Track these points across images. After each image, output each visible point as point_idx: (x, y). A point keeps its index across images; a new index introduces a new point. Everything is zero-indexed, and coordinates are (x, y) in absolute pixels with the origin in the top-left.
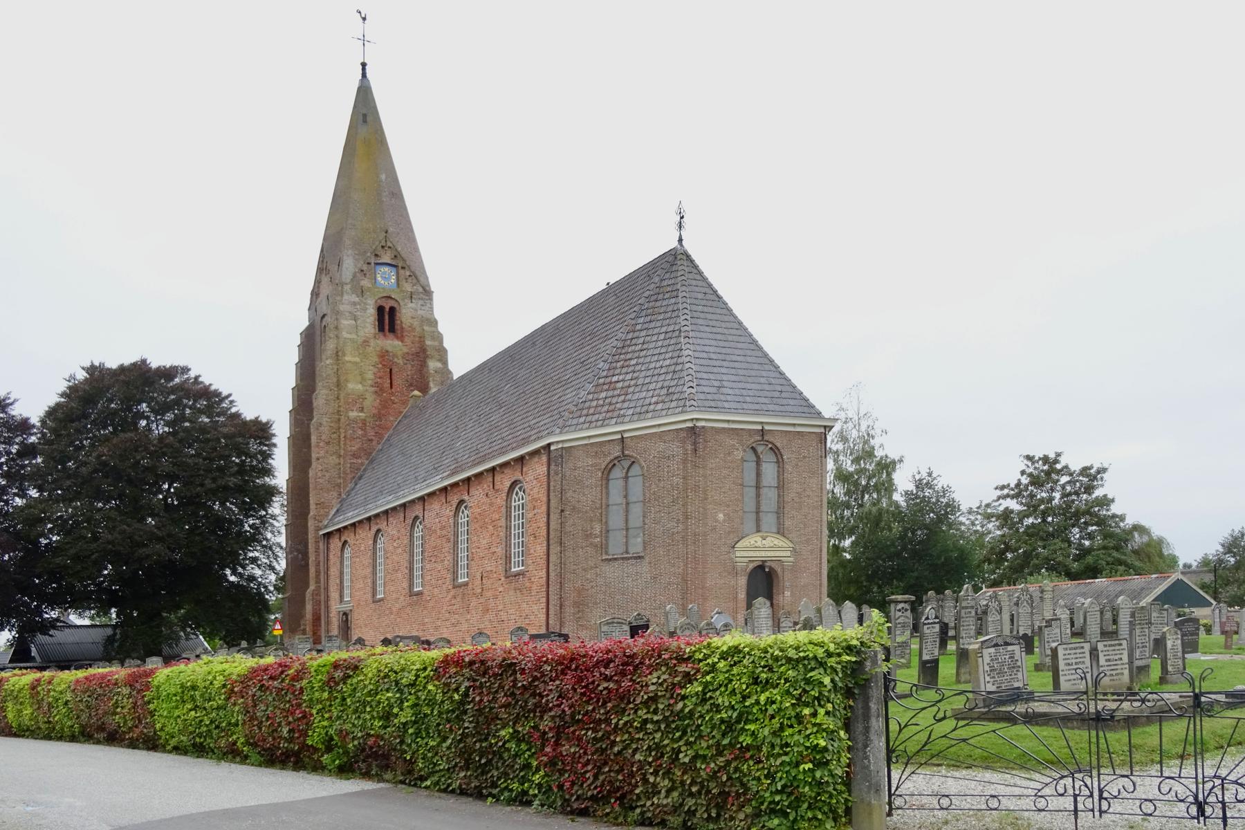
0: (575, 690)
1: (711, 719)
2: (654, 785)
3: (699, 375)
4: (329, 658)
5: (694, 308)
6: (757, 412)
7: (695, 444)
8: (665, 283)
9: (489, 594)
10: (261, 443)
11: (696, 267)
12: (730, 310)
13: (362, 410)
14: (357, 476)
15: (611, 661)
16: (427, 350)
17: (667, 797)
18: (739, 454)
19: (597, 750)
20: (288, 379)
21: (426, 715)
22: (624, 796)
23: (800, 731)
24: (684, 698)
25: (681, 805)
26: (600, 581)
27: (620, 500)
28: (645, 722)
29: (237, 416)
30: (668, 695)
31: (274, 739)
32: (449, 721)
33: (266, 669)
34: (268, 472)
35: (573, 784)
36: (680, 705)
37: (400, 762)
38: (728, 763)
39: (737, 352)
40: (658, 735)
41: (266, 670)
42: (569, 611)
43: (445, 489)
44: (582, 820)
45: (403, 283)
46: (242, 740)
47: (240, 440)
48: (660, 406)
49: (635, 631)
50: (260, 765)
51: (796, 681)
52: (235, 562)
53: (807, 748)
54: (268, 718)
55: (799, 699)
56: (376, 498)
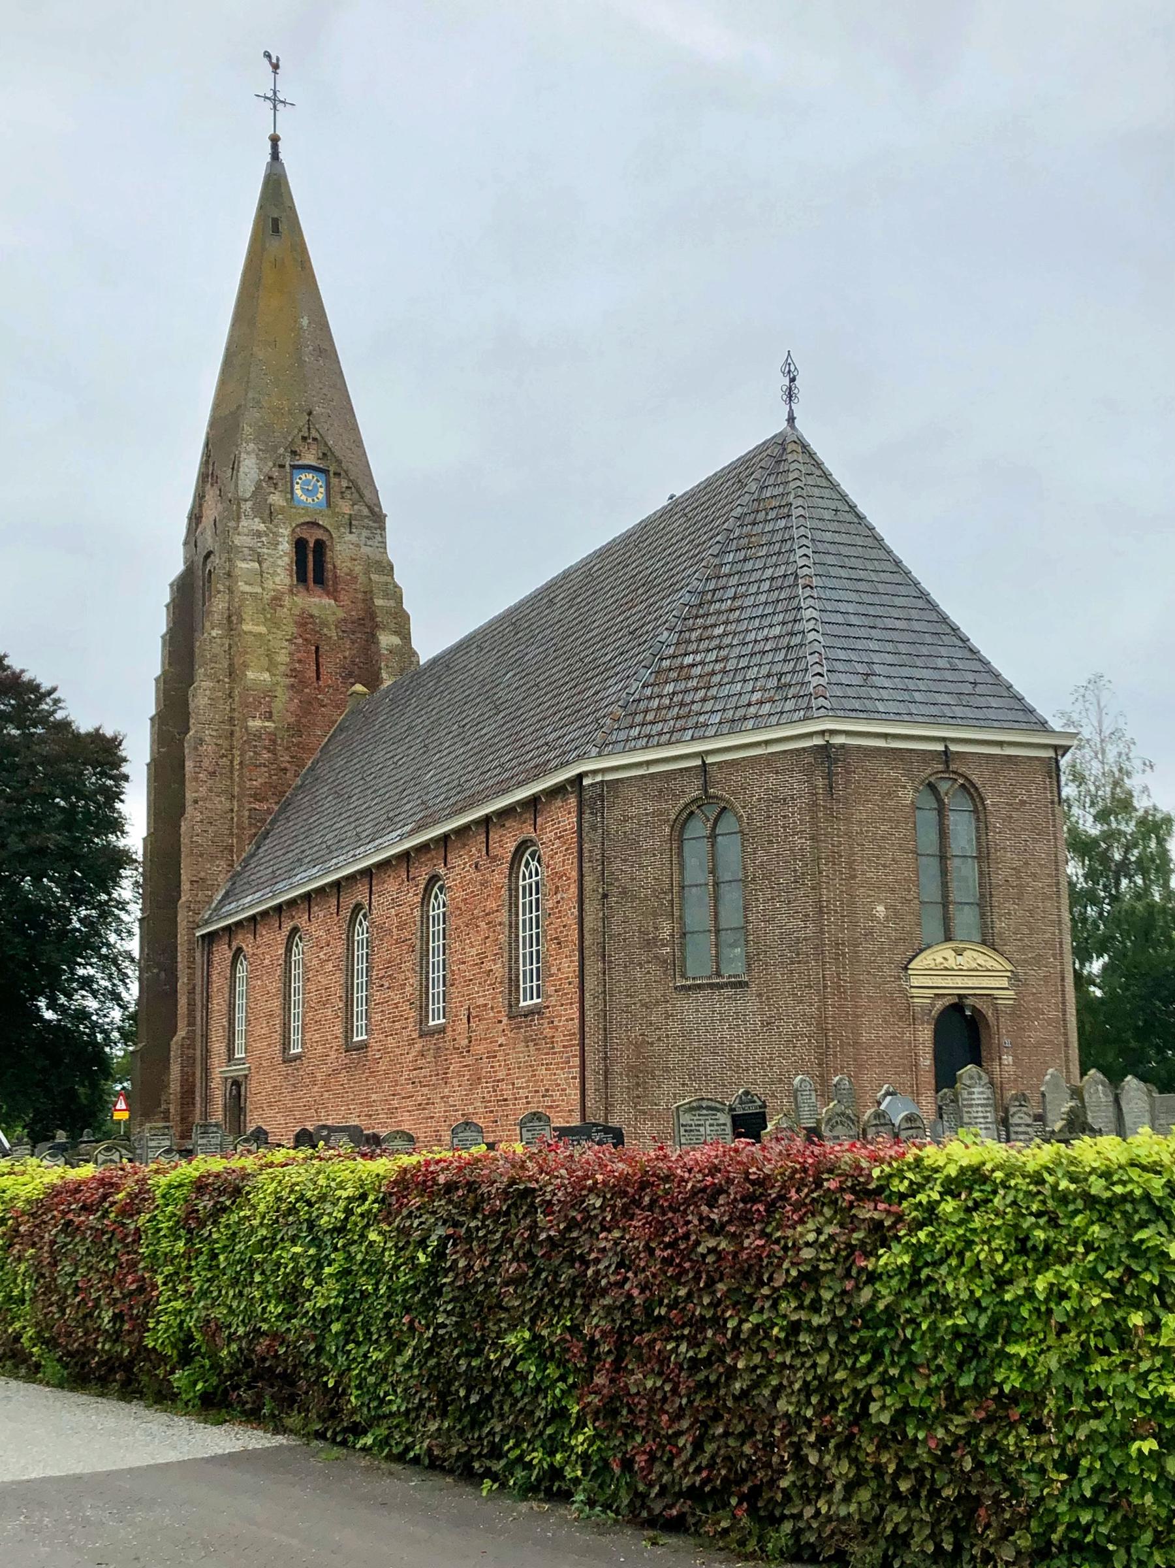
0: (651, 1252)
1: (933, 1327)
2: (820, 1471)
3: (831, 654)
4: (188, 1170)
5: (818, 535)
6: (934, 720)
7: (830, 775)
8: (768, 493)
9: (480, 1049)
10: (103, 774)
11: (818, 465)
12: (879, 540)
13: (269, 716)
14: (261, 831)
15: (720, 1191)
16: (375, 614)
17: (846, 1500)
18: (907, 796)
19: (699, 1386)
20: (151, 662)
21: (364, 1295)
22: (756, 1492)
23: (1125, 1365)
24: (873, 1277)
25: (878, 1520)
26: (674, 1027)
27: (705, 878)
28: (795, 1328)
29: (65, 725)
30: (840, 1271)
31: (87, 1333)
32: (408, 1309)
33: (76, 1188)
34: (116, 825)
35: (652, 1458)
36: (866, 1294)
37: (315, 1392)
38: (974, 1430)
39: (895, 613)
40: (823, 1360)
41: (77, 1190)
42: (620, 1082)
43: (405, 856)
44: (672, 1540)
45: (337, 499)
46: (30, 1332)
47: (69, 767)
48: (766, 709)
49: (749, 1124)
50: (60, 1386)
51: (1110, 1249)
52: (53, 983)
53: (1143, 1403)
54: (77, 1290)
55: (1118, 1290)
56: (290, 872)
